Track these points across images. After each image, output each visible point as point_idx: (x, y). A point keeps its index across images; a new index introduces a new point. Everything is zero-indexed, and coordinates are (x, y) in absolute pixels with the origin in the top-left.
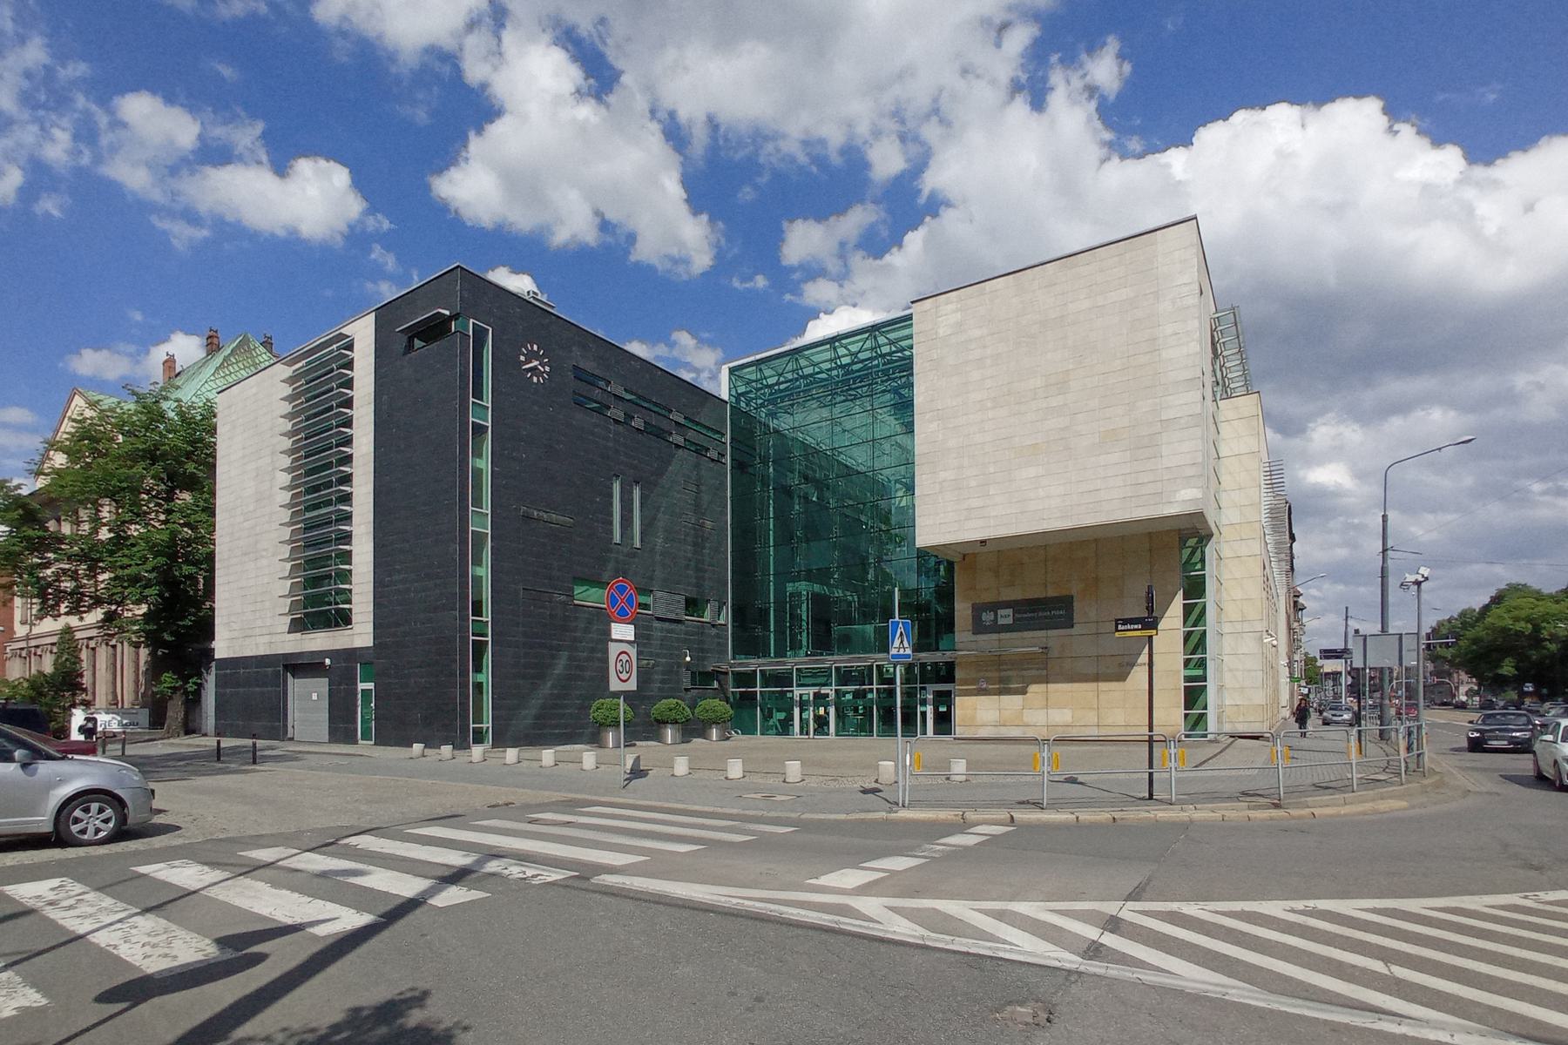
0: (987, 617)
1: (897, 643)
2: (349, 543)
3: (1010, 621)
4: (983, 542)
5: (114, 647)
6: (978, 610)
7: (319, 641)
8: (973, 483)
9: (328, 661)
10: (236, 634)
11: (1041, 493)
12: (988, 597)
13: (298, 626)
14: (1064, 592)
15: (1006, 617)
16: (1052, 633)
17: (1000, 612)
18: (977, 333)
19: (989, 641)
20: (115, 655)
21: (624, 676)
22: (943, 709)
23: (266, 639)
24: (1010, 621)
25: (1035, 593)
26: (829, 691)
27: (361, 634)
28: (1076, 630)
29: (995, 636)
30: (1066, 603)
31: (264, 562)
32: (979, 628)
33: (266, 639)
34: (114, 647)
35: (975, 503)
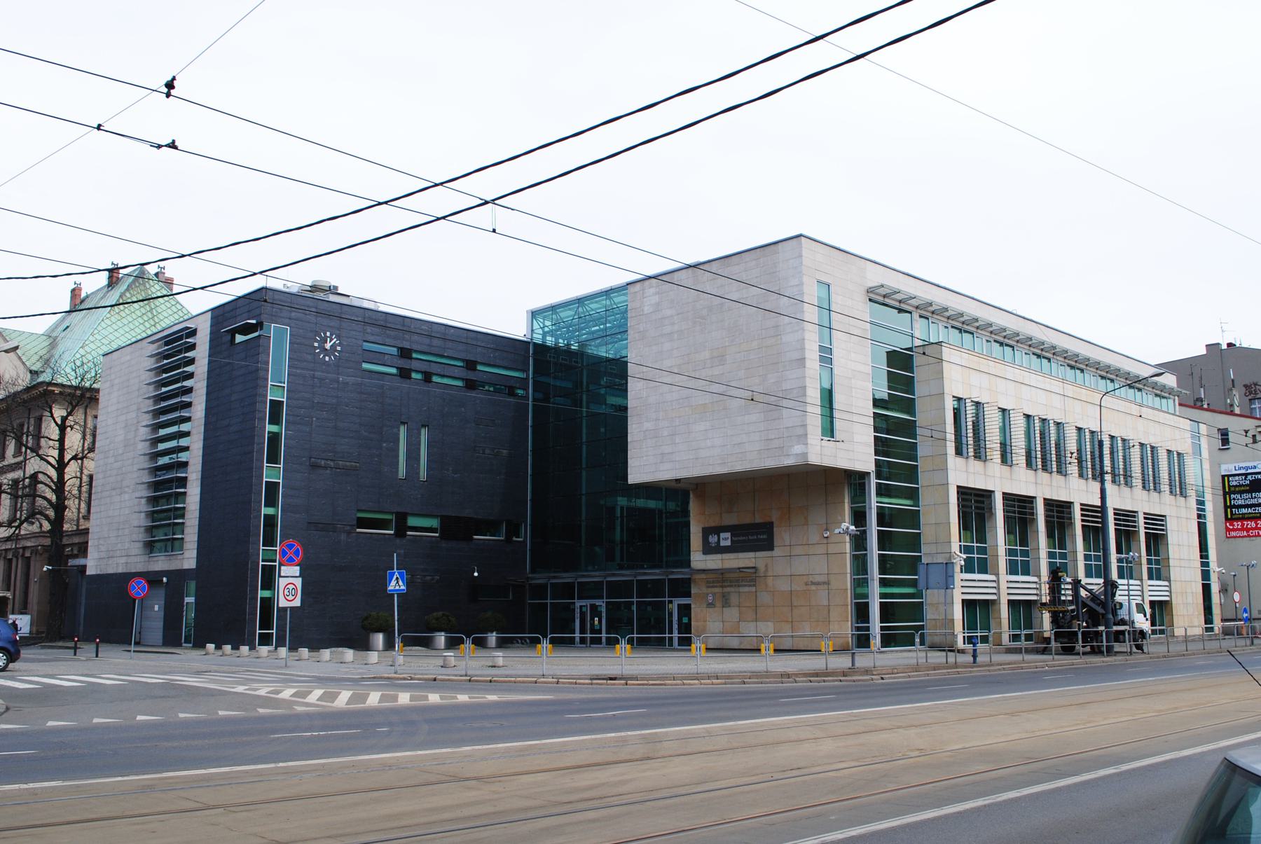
0: (713, 539)
1: (393, 583)
2: (185, 486)
3: (728, 543)
4: (678, 481)
5: (10, 560)
6: (707, 532)
7: (161, 563)
8: (666, 433)
9: (165, 580)
10: (103, 555)
11: (709, 443)
12: (712, 523)
13: (150, 546)
14: (768, 520)
15: (726, 539)
16: (759, 554)
17: (722, 535)
18: (668, 312)
19: (714, 562)
20: (10, 568)
21: (290, 598)
22: (685, 620)
23: (123, 560)
24: (728, 543)
25: (747, 520)
26: (601, 603)
27: (188, 559)
28: (777, 552)
29: (719, 556)
30: (768, 528)
31: (126, 496)
32: (708, 549)
33: (123, 560)
34: (10, 560)
35: (667, 449)
